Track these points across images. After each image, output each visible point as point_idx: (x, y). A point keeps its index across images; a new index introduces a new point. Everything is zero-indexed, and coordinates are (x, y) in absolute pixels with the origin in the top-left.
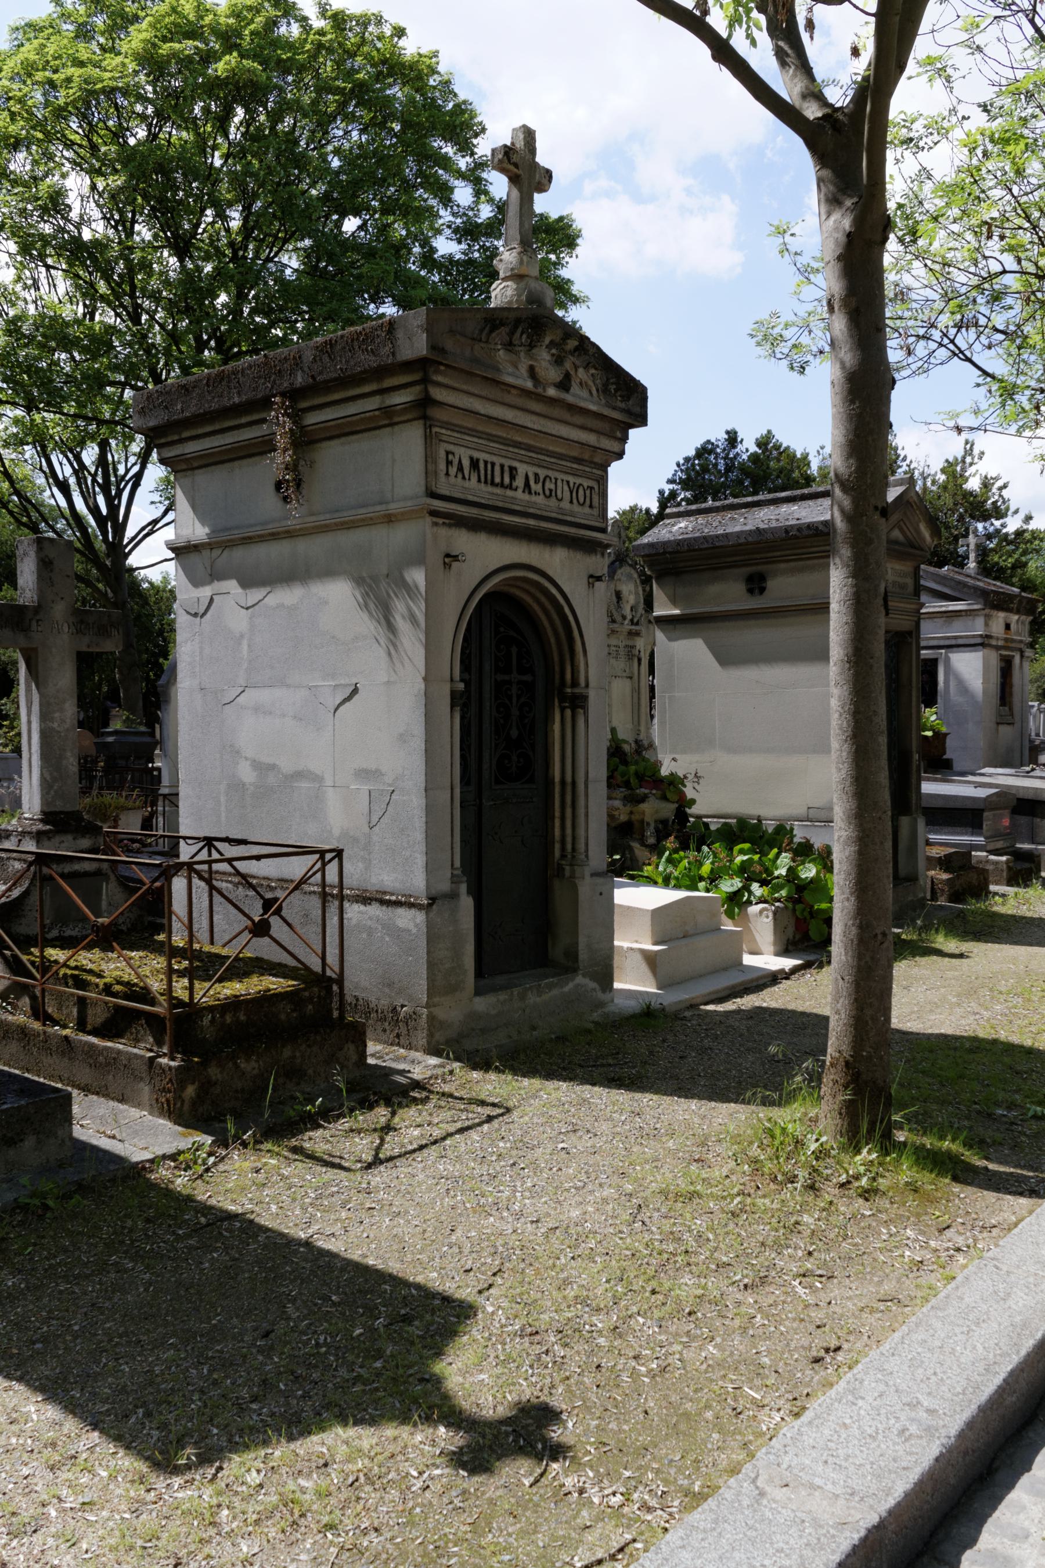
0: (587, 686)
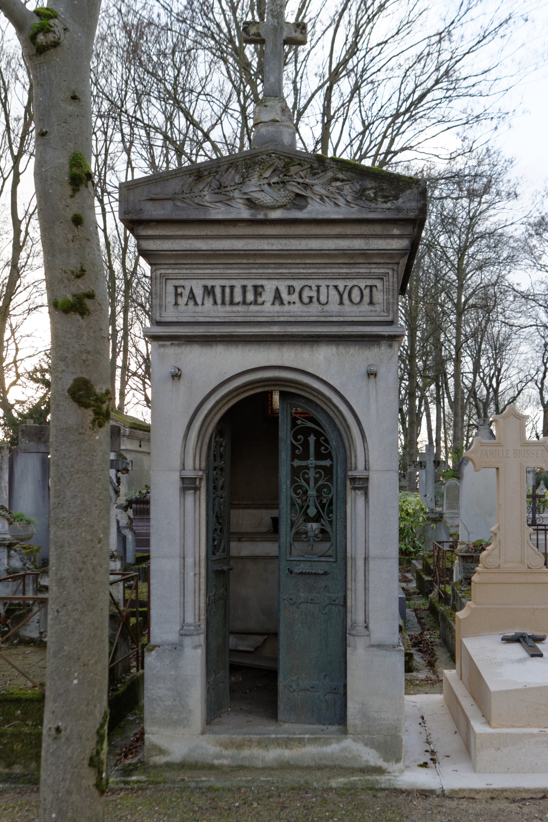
0: (366, 468)
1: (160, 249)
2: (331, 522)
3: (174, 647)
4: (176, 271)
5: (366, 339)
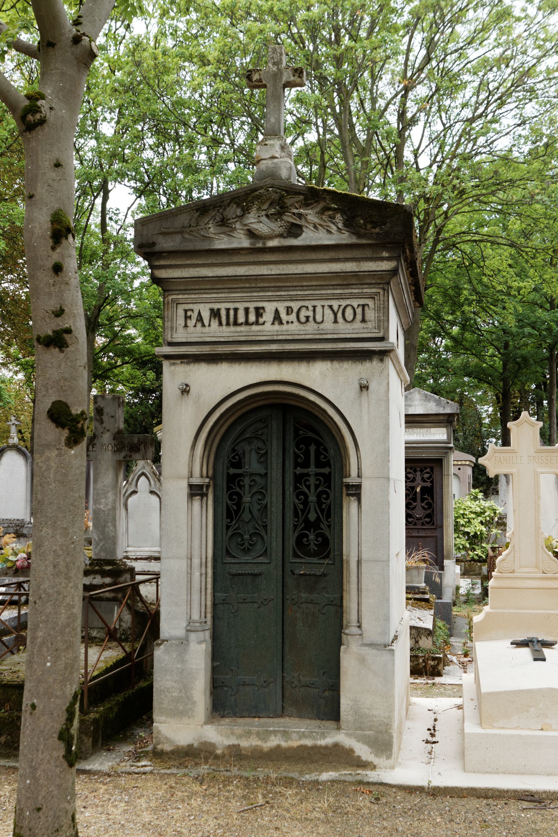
0: (359, 476)
1: (171, 277)
2: (329, 526)
3: (181, 641)
4: (186, 296)
5: (359, 354)
